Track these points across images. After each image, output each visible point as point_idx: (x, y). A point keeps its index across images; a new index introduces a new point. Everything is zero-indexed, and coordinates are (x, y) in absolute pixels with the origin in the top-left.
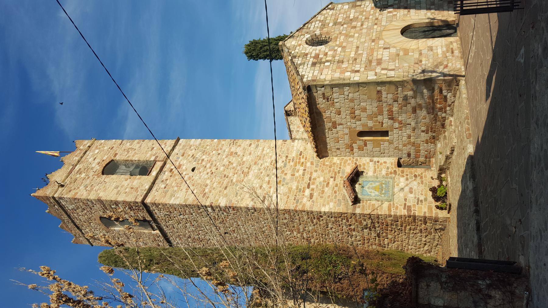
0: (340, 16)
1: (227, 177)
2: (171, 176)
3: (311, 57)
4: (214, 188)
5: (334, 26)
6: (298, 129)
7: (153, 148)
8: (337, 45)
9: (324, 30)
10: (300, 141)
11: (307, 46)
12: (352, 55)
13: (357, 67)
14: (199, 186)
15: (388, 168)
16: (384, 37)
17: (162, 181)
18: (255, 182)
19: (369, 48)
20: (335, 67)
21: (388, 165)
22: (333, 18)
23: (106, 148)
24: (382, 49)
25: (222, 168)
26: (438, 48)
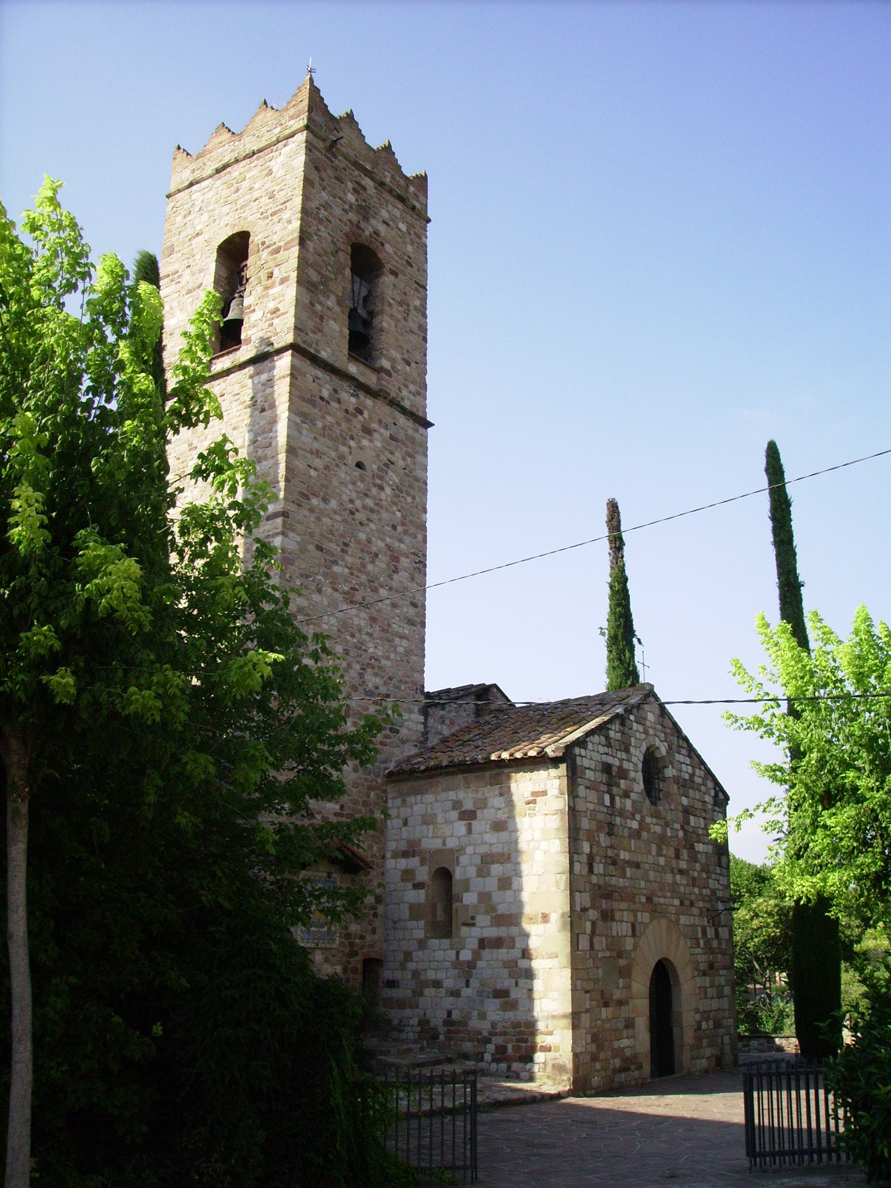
0: (702, 820)
1: (343, 551)
2: (347, 411)
3: (621, 760)
4: (319, 519)
5: (680, 808)
6: (447, 722)
7: (409, 364)
8: (643, 818)
9: (675, 787)
10: (421, 728)
11: (644, 748)
12: (624, 855)
13: (599, 868)
14: (325, 482)
15: (362, 937)
16: (655, 922)
17: (336, 391)
18: (333, 621)
19: (635, 891)
20: (600, 817)
21: (369, 938)
22: (699, 805)
23: (409, 248)
24: (632, 919)
25: (362, 536)
26: (631, 1040)
